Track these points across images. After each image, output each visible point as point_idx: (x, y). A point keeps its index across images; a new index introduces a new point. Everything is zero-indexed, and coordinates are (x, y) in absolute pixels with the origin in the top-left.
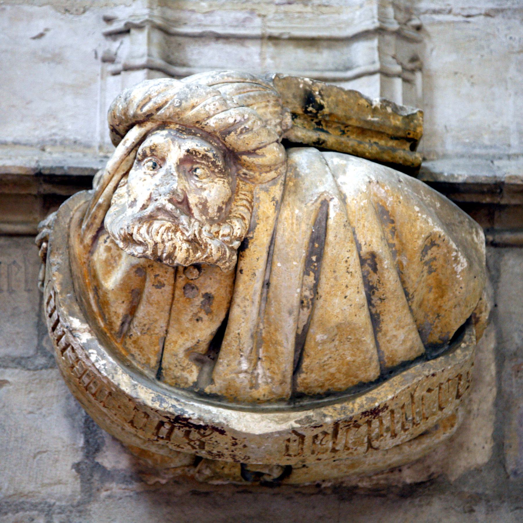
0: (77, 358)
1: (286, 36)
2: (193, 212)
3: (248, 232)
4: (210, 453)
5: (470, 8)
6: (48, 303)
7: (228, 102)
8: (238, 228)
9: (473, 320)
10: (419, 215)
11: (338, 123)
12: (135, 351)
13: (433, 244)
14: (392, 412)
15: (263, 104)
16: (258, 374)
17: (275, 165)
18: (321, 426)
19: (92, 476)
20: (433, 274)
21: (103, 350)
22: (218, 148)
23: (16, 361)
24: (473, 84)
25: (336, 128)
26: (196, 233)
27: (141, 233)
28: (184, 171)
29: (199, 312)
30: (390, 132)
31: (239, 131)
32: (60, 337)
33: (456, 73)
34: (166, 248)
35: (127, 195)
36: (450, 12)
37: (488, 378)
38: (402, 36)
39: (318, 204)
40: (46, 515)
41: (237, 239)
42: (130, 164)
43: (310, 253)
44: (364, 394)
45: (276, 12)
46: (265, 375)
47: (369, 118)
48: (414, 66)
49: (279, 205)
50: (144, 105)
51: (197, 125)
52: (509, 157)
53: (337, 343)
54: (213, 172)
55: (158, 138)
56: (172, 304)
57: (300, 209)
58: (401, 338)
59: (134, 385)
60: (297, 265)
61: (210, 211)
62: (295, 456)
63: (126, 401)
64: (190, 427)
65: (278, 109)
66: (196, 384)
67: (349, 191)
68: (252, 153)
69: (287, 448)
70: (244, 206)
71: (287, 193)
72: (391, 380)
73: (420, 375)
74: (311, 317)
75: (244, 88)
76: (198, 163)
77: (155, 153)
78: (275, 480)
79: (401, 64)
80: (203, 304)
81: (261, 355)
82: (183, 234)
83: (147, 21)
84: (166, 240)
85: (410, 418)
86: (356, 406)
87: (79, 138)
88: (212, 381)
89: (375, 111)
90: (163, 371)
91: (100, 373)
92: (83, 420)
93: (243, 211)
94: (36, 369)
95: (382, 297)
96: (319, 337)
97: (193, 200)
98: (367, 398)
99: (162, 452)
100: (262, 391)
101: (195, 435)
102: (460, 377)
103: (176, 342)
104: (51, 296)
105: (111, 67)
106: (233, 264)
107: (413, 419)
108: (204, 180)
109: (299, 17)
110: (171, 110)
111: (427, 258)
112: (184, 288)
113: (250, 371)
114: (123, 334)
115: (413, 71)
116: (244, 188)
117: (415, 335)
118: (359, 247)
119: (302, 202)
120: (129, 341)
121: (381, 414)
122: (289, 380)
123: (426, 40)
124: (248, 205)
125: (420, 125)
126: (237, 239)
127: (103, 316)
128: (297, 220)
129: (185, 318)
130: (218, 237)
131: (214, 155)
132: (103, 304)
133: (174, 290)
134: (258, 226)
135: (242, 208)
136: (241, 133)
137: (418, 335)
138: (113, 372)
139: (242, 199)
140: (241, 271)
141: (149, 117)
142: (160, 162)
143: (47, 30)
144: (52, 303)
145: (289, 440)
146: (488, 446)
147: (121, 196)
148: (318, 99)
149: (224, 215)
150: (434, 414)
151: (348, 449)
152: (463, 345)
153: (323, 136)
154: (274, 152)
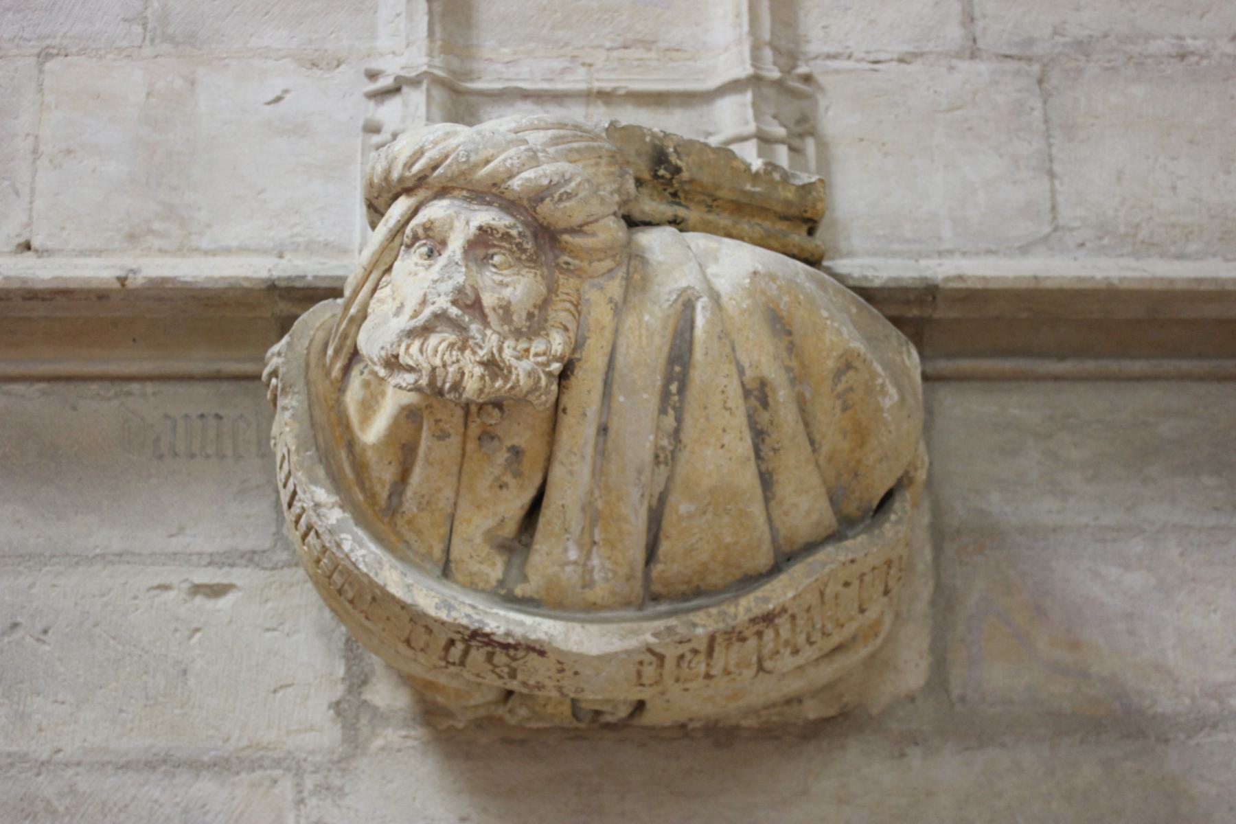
0: (324, 546)
1: (623, 92)
2: (489, 319)
3: (574, 350)
4: (525, 684)
5: (878, 51)
6: (281, 467)
7: (540, 155)
8: (558, 343)
9: (905, 481)
10: (829, 322)
11: (703, 194)
12: (411, 536)
13: (849, 366)
14: (793, 617)
15: (593, 161)
16: (593, 568)
17: (612, 248)
18: (689, 641)
19: (358, 719)
20: (849, 412)
21: (360, 533)
22: (525, 224)
23: (247, 556)
24: (886, 154)
25: (699, 202)
26: (495, 351)
27: (412, 353)
28: (476, 260)
29: (504, 474)
30: (779, 208)
31: (556, 196)
32: (299, 517)
33: (862, 140)
34: (450, 375)
35: (390, 300)
36: (850, 57)
37: (921, 567)
38: (786, 89)
39: (679, 306)
40: (296, 774)
41: (557, 359)
42: (394, 254)
43: (668, 381)
44: (750, 592)
45: (607, 60)
46: (603, 568)
47: (748, 187)
48: (804, 129)
49: (618, 310)
50: (413, 164)
51: (494, 190)
52: (940, 254)
53: (709, 516)
54: (519, 259)
55: (437, 210)
56: (461, 465)
57: (651, 314)
58: (804, 506)
59: (409, 586)
60: (650, 399)
61: (515, 318)
62: (651, 685)
63: (397, 609)
64: (494, 647)
65: (615, 169)
66: (501, 583)
67: (723, 285)
68: (578, 230)
69: (639, 674)
70: (568, 310)
71: (631, 290)
72: (791, 571)
73: (832, 562)
74: (670, 479)
75: (563, 137)
76: (495, 246)
77: (431, 233)
78: (622, 720)
79: (785, 126)
80: (509, 463)
81: (597, 537)
82: (474, 353)
83: (425, 72)
84: (449, 362)
85: (819, 626)
86: (741, 610)
87: (331, 239)
88: (525, 579)
89: (756, 177)
90: (453, 565)
91: (357, 568)
92: (343, 640)
93: (564, 317)
94: (273, 569)
95: (776, 446)
96: (684, 508)
97: (488, 300)
98: (756, 599)
99: (455, 684)
100: (599, 592)
101: (501, 658)
102: (889, 563)
103: (469, 521)
104: (284, 457)
105: (376, 139)
106: (553, 398)
107: (823, 626)
108: (505, 272)
109: (639, 66)
110: (454, 167)
111: (840, 388)
112: (479, 438)
113: (582, 562)
114: (392, 508)
115: (801, 136)
116: (568, 285)
117: (823, 504)
118: (741, 372)
119: (655, 303)
120: (401, 522)
121: (777, 621)
122: (639, 574)
123: (819, 96)
124: (572, 309)
125: (822, 200)
126: (557, 359)
127: (361, 484)
128: (648, 330)
129: (483, 485)
130: (527, 357)
131: (520, 233)
132: (360, 467)
133: (464, 442)
134: (589, 341)
135: (563, 314)
136: (560, 200)
137: (828, 503)
138: (377, 566)
139: (564, 301)
140: (564, 410)
141: (422, 179)
142: (439, 247)
143: (286, 91)
144: (286, 466)
145: (641, 663)
146: (925, 664)
147: (382, 301)
148: (674, 159)
149: (535, 324)
150: (852, 619)
151: (729, 673)
152: (893, 517)
153: (681, 212)
154: (612, 230)
